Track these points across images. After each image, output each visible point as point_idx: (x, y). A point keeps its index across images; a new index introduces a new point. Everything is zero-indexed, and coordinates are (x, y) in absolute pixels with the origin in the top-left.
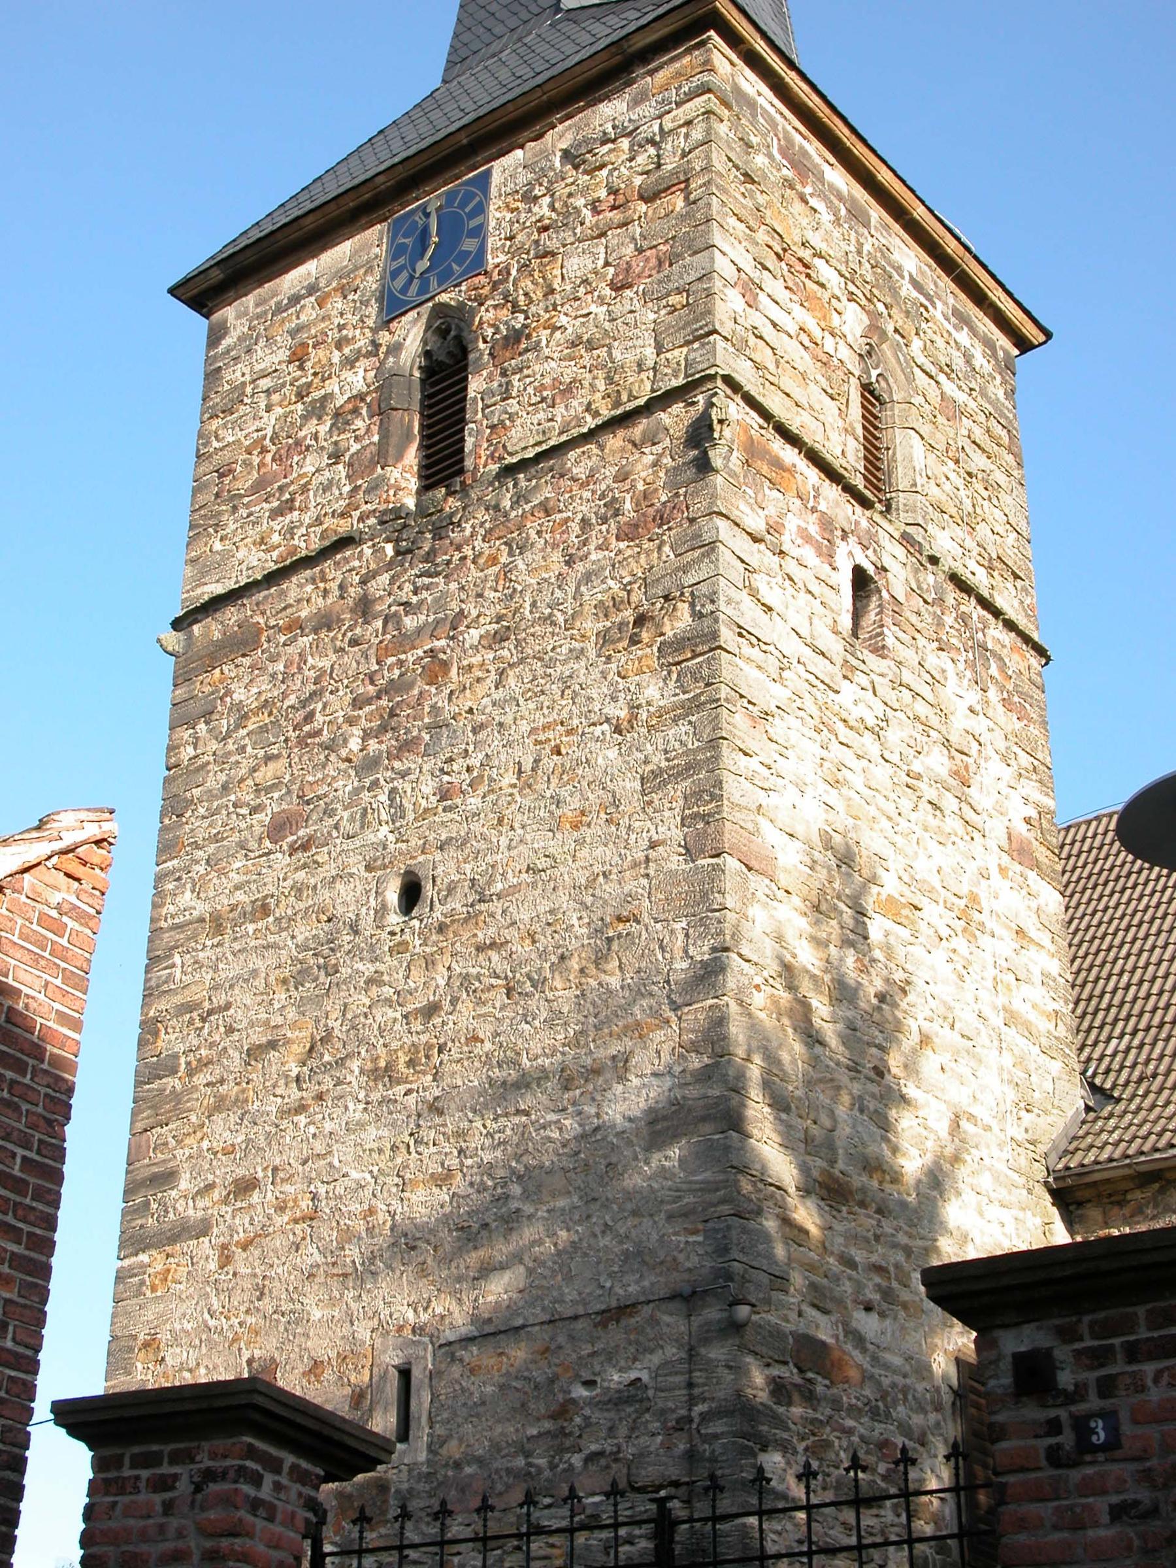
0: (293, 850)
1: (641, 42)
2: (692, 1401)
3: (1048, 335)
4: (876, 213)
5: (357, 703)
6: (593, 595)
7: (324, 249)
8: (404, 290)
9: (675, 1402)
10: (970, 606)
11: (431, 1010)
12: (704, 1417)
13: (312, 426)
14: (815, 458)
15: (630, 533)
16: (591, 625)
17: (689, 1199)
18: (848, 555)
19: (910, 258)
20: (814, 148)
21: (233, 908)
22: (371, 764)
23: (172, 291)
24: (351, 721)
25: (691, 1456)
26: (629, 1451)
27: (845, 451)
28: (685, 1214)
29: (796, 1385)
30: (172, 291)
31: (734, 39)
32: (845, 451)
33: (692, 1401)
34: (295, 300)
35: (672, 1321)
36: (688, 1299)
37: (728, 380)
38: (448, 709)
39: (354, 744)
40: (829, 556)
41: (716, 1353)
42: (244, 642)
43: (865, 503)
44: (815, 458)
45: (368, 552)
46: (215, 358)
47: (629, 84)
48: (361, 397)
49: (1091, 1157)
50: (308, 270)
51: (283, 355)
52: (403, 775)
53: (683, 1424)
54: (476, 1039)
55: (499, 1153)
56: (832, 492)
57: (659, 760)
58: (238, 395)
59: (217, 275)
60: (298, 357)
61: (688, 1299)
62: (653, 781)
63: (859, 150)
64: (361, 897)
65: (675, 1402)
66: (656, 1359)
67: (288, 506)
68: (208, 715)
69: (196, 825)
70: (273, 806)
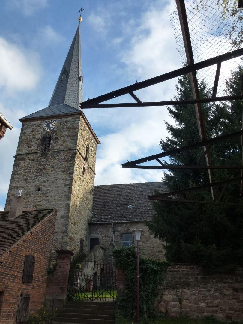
0: (27, 182)
1: (74, 114)
2: (62, 241)
3: (100, 143)
4: (90, 132)
5: (36, 169)
6: (62, 166)
7: (37, 121)
8: (46, 129)
9: (61, 241)
10: (91, 169)
11: (40, 201)
12: (63, 243)
13: (33, 139)
14: (82, 156)
15: (67, 161)
16: (61, 169)
17: (64, 224)
18: (83, 166)
19: (91, 136)
20: (86, 126)
21: (19, 186)
22: (36, 176)
23: (19, 120)
24: (35, 171)
25: (62, 246)
26: (56, 245)
27: (84, 156)
28: (64, 225)
29: (40, 123)
30: (19, 120)
31: (82, 116)
32: (84, 156)
33: (62, 241)
34: (33, 125)
35: (62, 234)
36: (63, 233)
37: (78, 150)
38: (46, 173)
39: (35, 173)
40: (82, 166)
41: (65, 237)
42: (24, 159)
43: (84, 160)
44: (82, 156)
45: (38, 155)
46: (23, 128)
47: (72, 117)
48: (39, 138)
49: (93, 221)
50: (35, 122)
51: (31, 130)
52: (40, 178)
53: (61, 243)
54: (45, 205)
55: (55, 238)
56: (83, 160)
57: (66, 184)
58: (26, 133)
59: (24, 120)
60: (33, 131)
61: (63, 233)
62: (66, 185)
63: (90, 126)
64: (33, 189)
65: (61, 241)
66: (59, 237)
67: (30, 147)
68: (19, 165)
69: (16, 177)
70: (25, 177)
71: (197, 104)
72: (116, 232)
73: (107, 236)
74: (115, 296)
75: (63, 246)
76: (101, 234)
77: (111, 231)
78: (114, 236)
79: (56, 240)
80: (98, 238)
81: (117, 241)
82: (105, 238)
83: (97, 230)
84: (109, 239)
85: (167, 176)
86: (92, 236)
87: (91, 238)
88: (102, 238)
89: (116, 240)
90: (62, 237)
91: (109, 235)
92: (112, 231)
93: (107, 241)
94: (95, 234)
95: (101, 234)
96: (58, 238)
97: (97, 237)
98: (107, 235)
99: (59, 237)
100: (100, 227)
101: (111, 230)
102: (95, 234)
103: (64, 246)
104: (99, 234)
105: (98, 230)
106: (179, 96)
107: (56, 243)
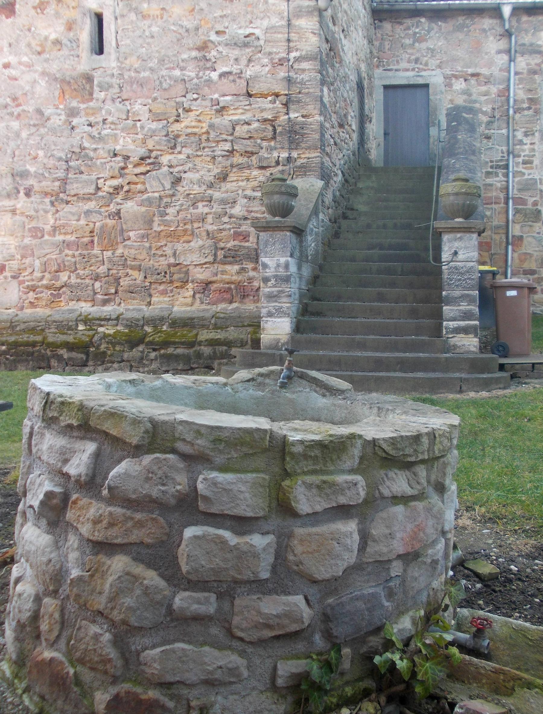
2: (289, 50)
12: (297, 60)
26: (249, 73)
33: (289, 50)
53: (281, 62)
71: (444, 308)
72: (523, 54)
73: (473, 75)
74: (444, 293)
75: (300, 77)
76: (439, 67)
77: (493, 52)
78: (516, 73)
79: (246, 45)
80: (426, 86)
81: (531, 100)
82: (459, 85)
83: (417, 44)
84: (484, 88)
85: (9, 678)
86: (390, 74)
87: (386, 87)
88: (449, 85)
89: (522, 95)
90: (284, 23)
91: (484, 71)
92: (499, 52)
93: (474, 97)
94: (404, 65)
95: (439, 67)
96: (257, 32)
97: (421, 81)
98: (470, 71)
99: (265, 23)
100: (429, 31)
101: (493, 45)
102: (404, 65)
103: (302, 83)
104: (426, 64)
105: (424, 45)
106: (394, 476)
107: (250, 61)
